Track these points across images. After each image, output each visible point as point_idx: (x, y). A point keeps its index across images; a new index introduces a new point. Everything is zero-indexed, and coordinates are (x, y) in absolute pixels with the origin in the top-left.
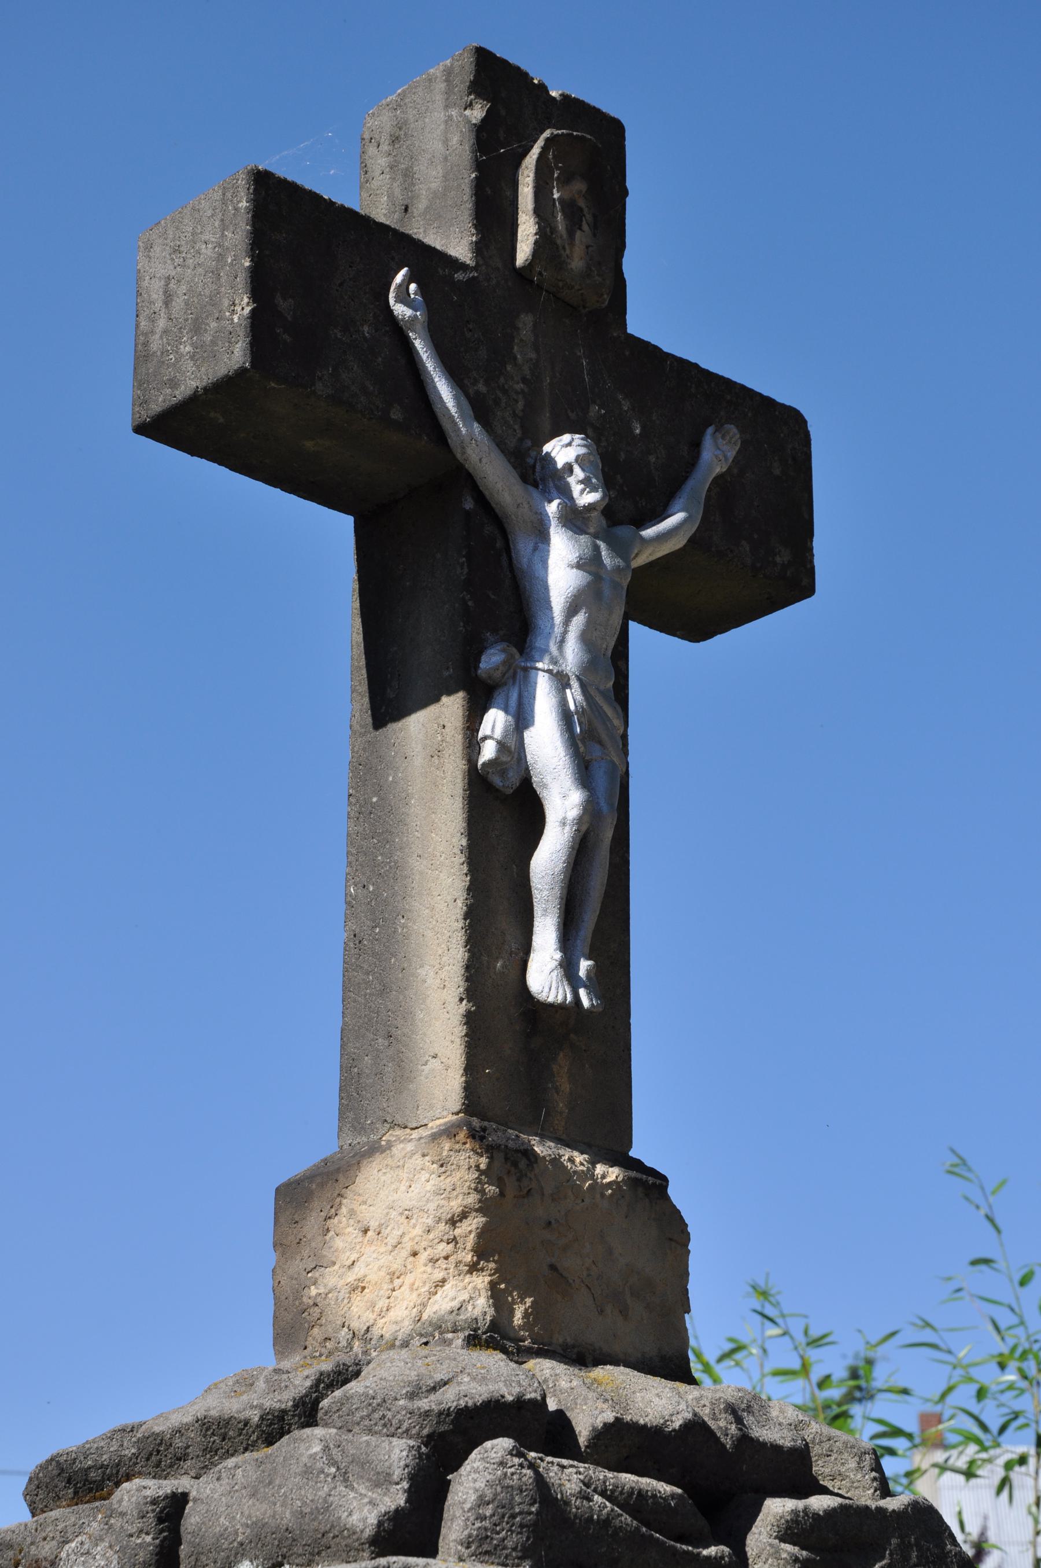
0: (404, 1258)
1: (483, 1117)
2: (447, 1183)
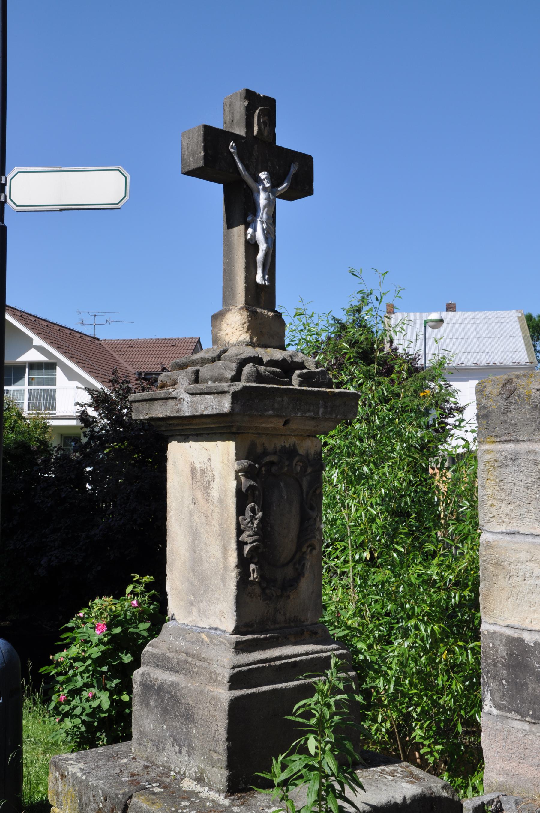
0: (235, 329)
1: (248, 305)
2: (242, 317)
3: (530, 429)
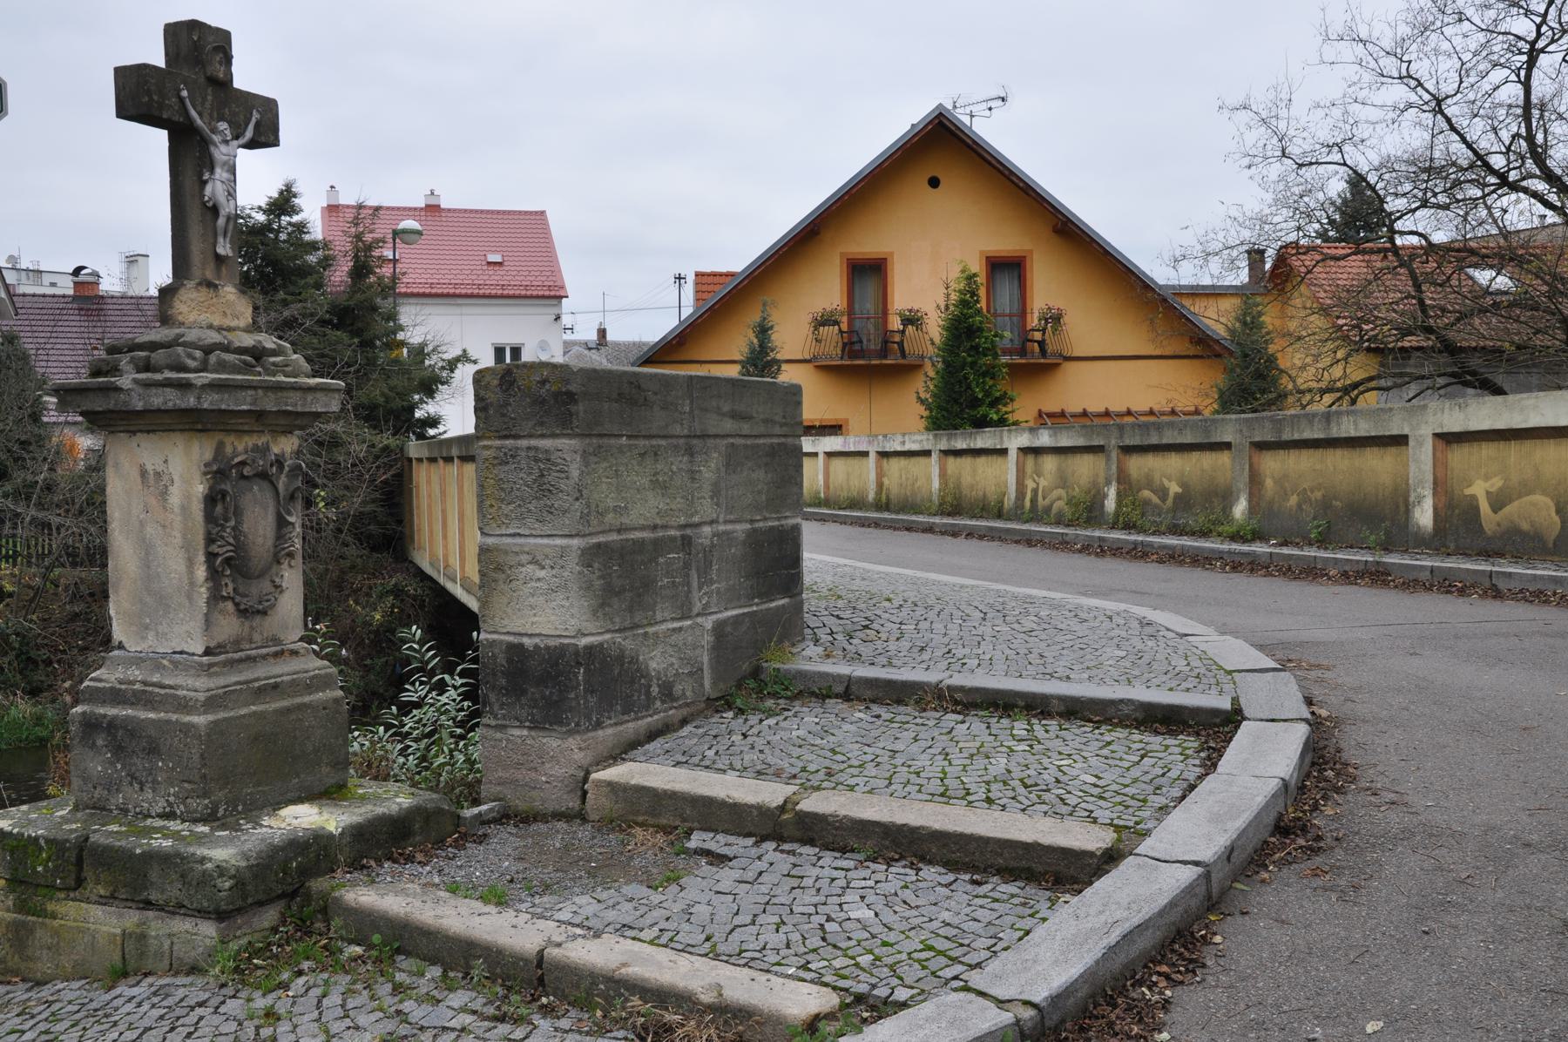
3: (531, 424)
